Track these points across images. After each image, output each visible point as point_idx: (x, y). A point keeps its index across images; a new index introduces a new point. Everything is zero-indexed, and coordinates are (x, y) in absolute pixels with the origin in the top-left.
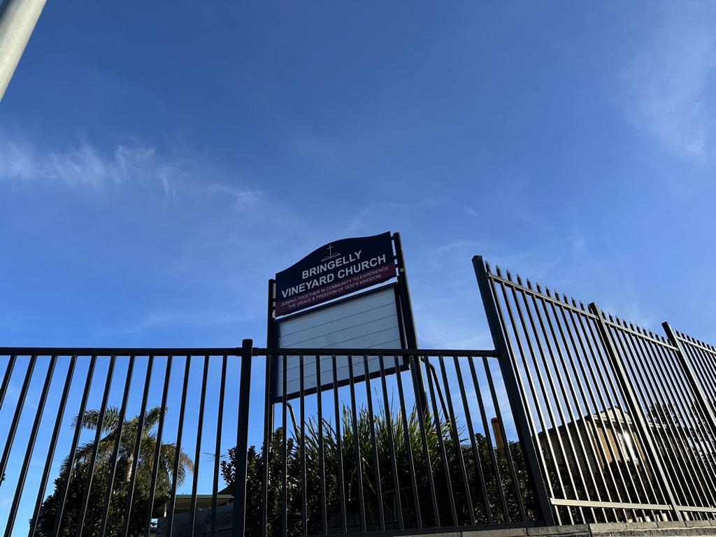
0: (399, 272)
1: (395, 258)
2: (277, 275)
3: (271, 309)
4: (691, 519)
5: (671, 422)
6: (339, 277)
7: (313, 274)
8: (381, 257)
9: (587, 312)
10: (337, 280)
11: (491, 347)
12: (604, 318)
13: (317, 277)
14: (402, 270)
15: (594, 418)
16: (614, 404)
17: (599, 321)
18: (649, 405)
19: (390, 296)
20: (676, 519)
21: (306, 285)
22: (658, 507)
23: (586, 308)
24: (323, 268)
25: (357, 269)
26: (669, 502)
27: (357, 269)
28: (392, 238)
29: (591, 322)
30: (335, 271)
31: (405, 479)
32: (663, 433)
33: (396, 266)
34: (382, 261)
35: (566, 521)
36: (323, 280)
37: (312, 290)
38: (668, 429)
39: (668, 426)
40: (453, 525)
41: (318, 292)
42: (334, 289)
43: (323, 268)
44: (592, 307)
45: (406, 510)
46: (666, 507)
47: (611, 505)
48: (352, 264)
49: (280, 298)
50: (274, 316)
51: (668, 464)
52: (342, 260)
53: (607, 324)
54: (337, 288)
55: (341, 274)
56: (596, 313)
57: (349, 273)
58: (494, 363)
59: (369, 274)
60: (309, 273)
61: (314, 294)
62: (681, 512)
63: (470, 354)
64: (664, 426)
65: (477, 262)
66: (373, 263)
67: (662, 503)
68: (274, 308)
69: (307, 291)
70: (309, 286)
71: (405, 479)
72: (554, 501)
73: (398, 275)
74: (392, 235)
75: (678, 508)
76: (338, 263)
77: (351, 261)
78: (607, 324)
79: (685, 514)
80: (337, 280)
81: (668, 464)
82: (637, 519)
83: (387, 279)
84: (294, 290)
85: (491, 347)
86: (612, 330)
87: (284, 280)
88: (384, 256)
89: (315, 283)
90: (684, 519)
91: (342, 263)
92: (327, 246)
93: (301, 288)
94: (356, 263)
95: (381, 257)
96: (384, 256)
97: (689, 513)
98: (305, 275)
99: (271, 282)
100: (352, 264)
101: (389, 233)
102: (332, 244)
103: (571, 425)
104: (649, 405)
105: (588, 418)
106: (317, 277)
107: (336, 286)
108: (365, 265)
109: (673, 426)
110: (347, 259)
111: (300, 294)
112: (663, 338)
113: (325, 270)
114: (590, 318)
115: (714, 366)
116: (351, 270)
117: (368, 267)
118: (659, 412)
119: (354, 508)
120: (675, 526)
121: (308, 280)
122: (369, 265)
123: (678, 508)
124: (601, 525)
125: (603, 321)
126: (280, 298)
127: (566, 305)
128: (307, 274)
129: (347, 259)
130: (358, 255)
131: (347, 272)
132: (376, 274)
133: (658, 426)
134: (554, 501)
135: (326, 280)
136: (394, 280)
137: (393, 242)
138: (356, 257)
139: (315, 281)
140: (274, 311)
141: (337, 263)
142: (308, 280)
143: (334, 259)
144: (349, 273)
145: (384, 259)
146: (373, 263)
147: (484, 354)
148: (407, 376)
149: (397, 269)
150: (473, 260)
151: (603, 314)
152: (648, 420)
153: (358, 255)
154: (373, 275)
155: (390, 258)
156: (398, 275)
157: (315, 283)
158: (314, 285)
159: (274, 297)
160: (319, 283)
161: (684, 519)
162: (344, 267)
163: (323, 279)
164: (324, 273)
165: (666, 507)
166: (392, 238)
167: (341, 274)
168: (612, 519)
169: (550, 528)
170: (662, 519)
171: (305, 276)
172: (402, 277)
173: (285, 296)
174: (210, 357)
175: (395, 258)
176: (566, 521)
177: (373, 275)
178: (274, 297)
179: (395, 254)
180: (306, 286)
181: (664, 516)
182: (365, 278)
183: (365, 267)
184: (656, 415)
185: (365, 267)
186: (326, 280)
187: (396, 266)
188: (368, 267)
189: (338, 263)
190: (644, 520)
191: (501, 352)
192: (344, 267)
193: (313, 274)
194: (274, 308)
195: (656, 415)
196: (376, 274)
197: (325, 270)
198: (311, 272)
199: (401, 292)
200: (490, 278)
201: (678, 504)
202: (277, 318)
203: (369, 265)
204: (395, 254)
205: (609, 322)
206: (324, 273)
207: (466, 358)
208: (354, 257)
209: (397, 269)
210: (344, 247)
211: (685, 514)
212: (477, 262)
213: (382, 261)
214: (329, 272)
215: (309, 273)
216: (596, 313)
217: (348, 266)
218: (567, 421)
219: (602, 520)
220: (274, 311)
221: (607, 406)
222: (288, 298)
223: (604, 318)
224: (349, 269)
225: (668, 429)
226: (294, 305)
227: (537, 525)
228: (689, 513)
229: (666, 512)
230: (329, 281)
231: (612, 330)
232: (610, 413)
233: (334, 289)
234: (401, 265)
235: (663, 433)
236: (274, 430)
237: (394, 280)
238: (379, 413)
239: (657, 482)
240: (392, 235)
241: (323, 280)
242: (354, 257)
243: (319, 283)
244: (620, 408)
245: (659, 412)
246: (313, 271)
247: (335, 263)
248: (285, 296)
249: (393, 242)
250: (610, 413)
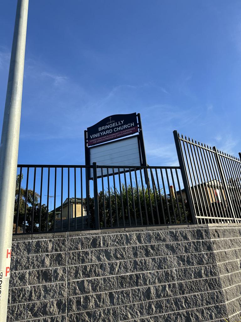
0: (140, 130)
1: (138, 124)
2: (88, 128)
3: (86, 143)
4: (240, 222)
5: (236, 186)
6: (112, 130)
7: (103, 129)
8: (132, 124)
9: (212, 151)
10: (113, 132)
11: (179, 166)
12: (218, 152)
13: (105, 130)
14: (141, 130)
15: (207, 183)
16: (214, 178)
17: (216, 154)
18: (229, 178)
19: (136, 140)
20: (234, 222)
21: (100, 134)
22: (226, 218)
23: (212, 148)
24: (107, 127)
25: (122, 128)
26: (233, 217)
27: (122, 128)
28: (137, 116)
29: (213, 154)
30: (113, 128)
31: (143, 208)
32: (233, 190)
33: (138, 128)
34: (132, 125)
35: (200, 223)
36: (107, 132)
37: (103, 136)
38: (235, 188)
39: (235, 187)
40: (153, 224)
41: (106, 137)
42: (112, 136)
43: (107, 127)
44: (214, 148)
45: (144, 218)
46: (232, 219)
47: (211, 218)
48: (120, 126)
49: (89, 139)
50: (87, 146)
51: (234, 203)
52: (116, 124)
53: (219, 155)
54: (114, 136)
55: (115, 130)
56: (215, 151)
57: (119, 129)
58: (179, 171)
59: (127, 130)
60: (102, 128)
61: (104, 137)
62: (237, 220)
63: (171, 168)
64: (233, 187)
65: (175, 133)
66: (129, 126)
67: (231, 217)
68: (87, 143)
69: (101, 136)
70: (102, 134)
71: (143, 208)
72: (197, 217)
73: (139, 131)
74: (137, 114)
75: (236, 219)
76: (114, 125)
77: (119, 124)
78: (219, 155)
79: (238, 221)
80: (113, 132)
81: (234, 203)
82: (219, 223)
83: (135, 133)
84: (95, 136)
85: (179, 166)
86: (220, 156)
87: (91, 131)
88: (133, 123)
89: (104, 133)
90: (237, 222)
91: (116, 125)
92: (109, 117)
93: (98, 135)
94: (122, 125)
95: (132, 124)
96: (133, 123)
97: (239, 220)
98: (100, 129)
99: (85, 131)
100: (120, 126)
101: (136, 113)
102: (111, 116)
103: (199, 185)
104: (229, 178)
105: (205, 183)
106: (105, 130)
107: (113, 135)
108: (125, 126)
109: (237, 187)
110: (118, 123)
111: (98, 137)
112: (238, 159)
113: (108, 127)
114: (213, 152)
115: (240, 207)
116: (120, 128)
117: (127, 127)
118: (232, 181)
119: (127, 218)
120: (234, 224)
121: (101, 131)
122: (127, 127)
123: (236, 219)
124: (211, 224)
125: (217, 153)
126: (89, 139)
127: (205, 148)
128: (101, 129)
129: (118, 123)
130: (122, 122)
131: (118, 129)
132: (130, 131)
133: (231, 187)
134: (197, 217)
135: (109, 132)
136: (137, 134)
137: (137, 117)
138: (121, 123)
139: (104, 132)
140: (87, 144)
141: (113, 125)
142: (101, 131)
143: (112, 123)
144: (119, 129)
145: (133, 124)
146: (129, 126)
147: (176, 168)
148: (143, 170)
149: (139, 129)
150: (173, 132)
151: (218, 151)
152: (228, 184)
153: (122, 122)
154: (129, 131)
155: (136, 124)
156: (139, 131)
157: (104, 133)
158: (104, 134)
159: (87, 138)
160: (106, 133)
161: (237, 222)
162: (116, 127)
163: (107, 131)
164: (108, 129)
165: (232, 219)
166: (137, 116)
167: (115, 130)
168: (214, 222)
169: (195, 225)
170: (230, 222)
171: (100, 130)
172: (141, 133)
173: (92, 138)
174: (76, 168)
175: (138, 124)
176: (204, 223)
177: (129, 131)
178: (87, 138)
179: (138, 123)
180: (100, 134)
181: (231, 221)
182: (125, 132)
183: (125, 127)
184: (231, 182)
185: (125, 127)
186: (109, 132)
187: (138, 128)
188: (127, 127)
189: (114, 125)
190: (221, 223)
191: (182, 167)
192: (116, 127)
193: (103, 129)
194: (87, 143)
195: (231, 182)
196: (130, 131)
197: (108, 127)
198: (107, 132)
199: (140, 138)
200: (179, 139)
201: (236, 218)
202: (89, 147)
203: (127, 127)
204: (138, 123)
205: (220, 154)
206: (108, 129)
207: (170, 169)
208: (121, 123)
209: (139, 129)
210: (116, 118)
211: (238, 221)
212: (175, 133)
213: (132, 125)
214: (110, 128)
215: (102, 128)
216: (215, 151)
217: (118, 126)
218: (197, 184)
219: (211, 222)
220: (87, 144)
221: (212, 179)
222: (93, 139)
223: (218, 152)
224: (119, 128)
225: (235, 188)
226: (95, 142)
227: (191, 224)
228: (239, 220)
229: (232, 220)
230: (110, 132)
231: (220, 156)
232: (212, 182)
233: (112, 136)
234: (140, 127)
235: (233, 190)
236: (99, 192)
237: (137, 134)
238: (134, 186)
239: (229, 209)
240: (137, 114)
241: (107, 132)
242: (121, 123)
243: (106, 133)
244: (219, 181)
245: (232, 181)
246: (103, 128)
247: (113, 125)
248: (92, 138)
249: (137, 117)
250: (212, 182)
